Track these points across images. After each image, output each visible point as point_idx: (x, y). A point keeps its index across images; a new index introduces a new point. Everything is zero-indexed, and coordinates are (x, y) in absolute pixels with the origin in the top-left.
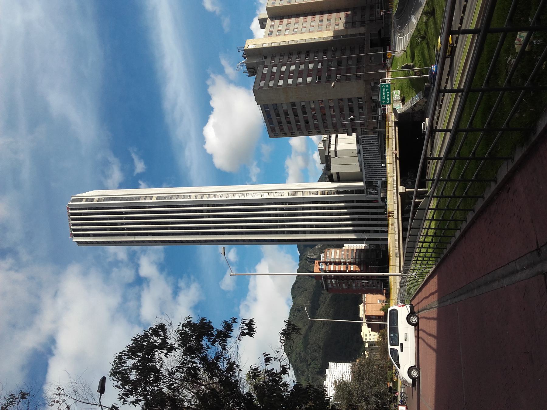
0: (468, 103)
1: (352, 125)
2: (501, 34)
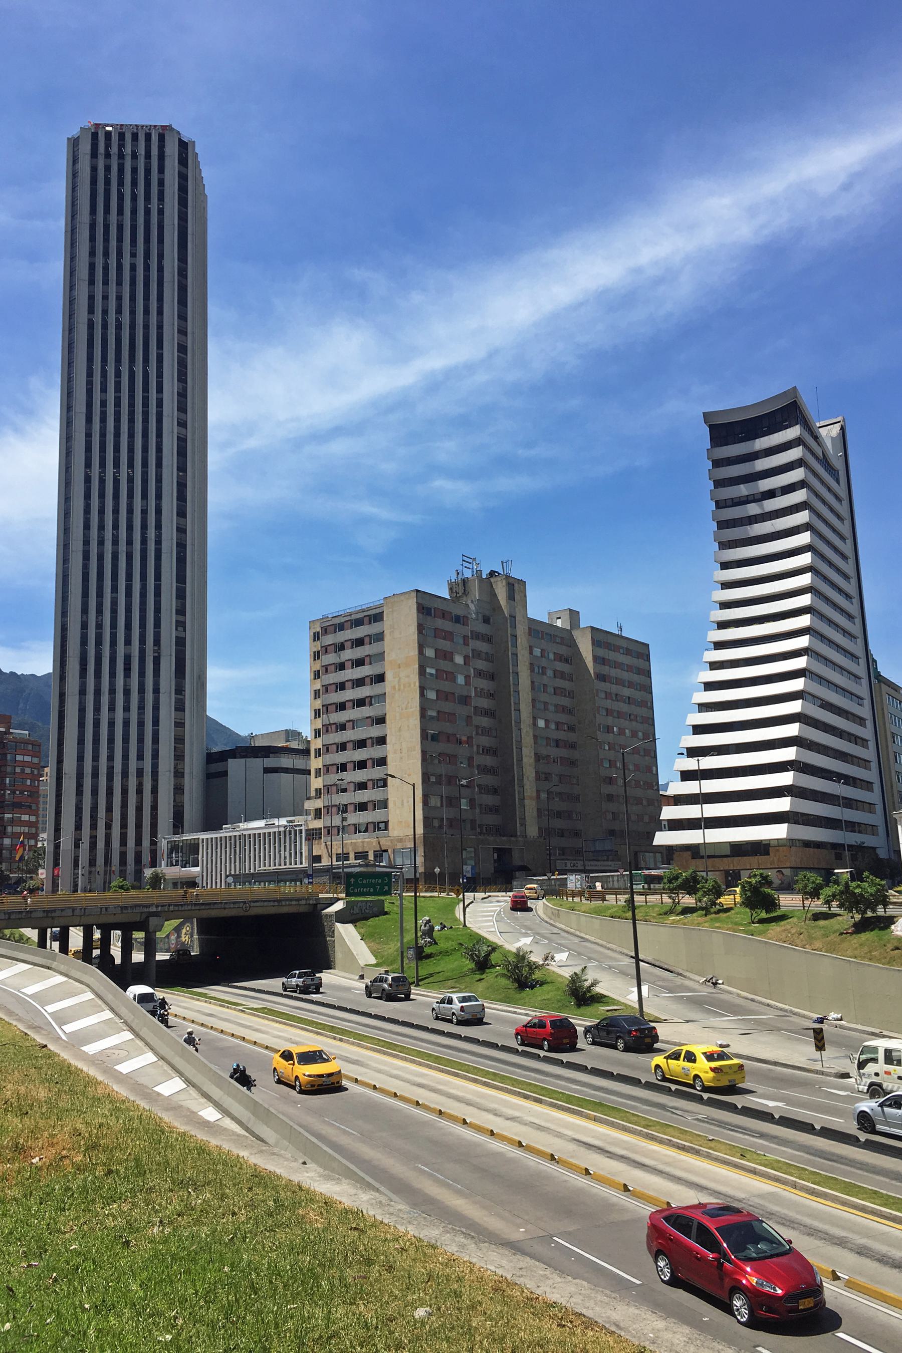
0: (243, 1132)
1: (451, 800)
2: (641, 963)
